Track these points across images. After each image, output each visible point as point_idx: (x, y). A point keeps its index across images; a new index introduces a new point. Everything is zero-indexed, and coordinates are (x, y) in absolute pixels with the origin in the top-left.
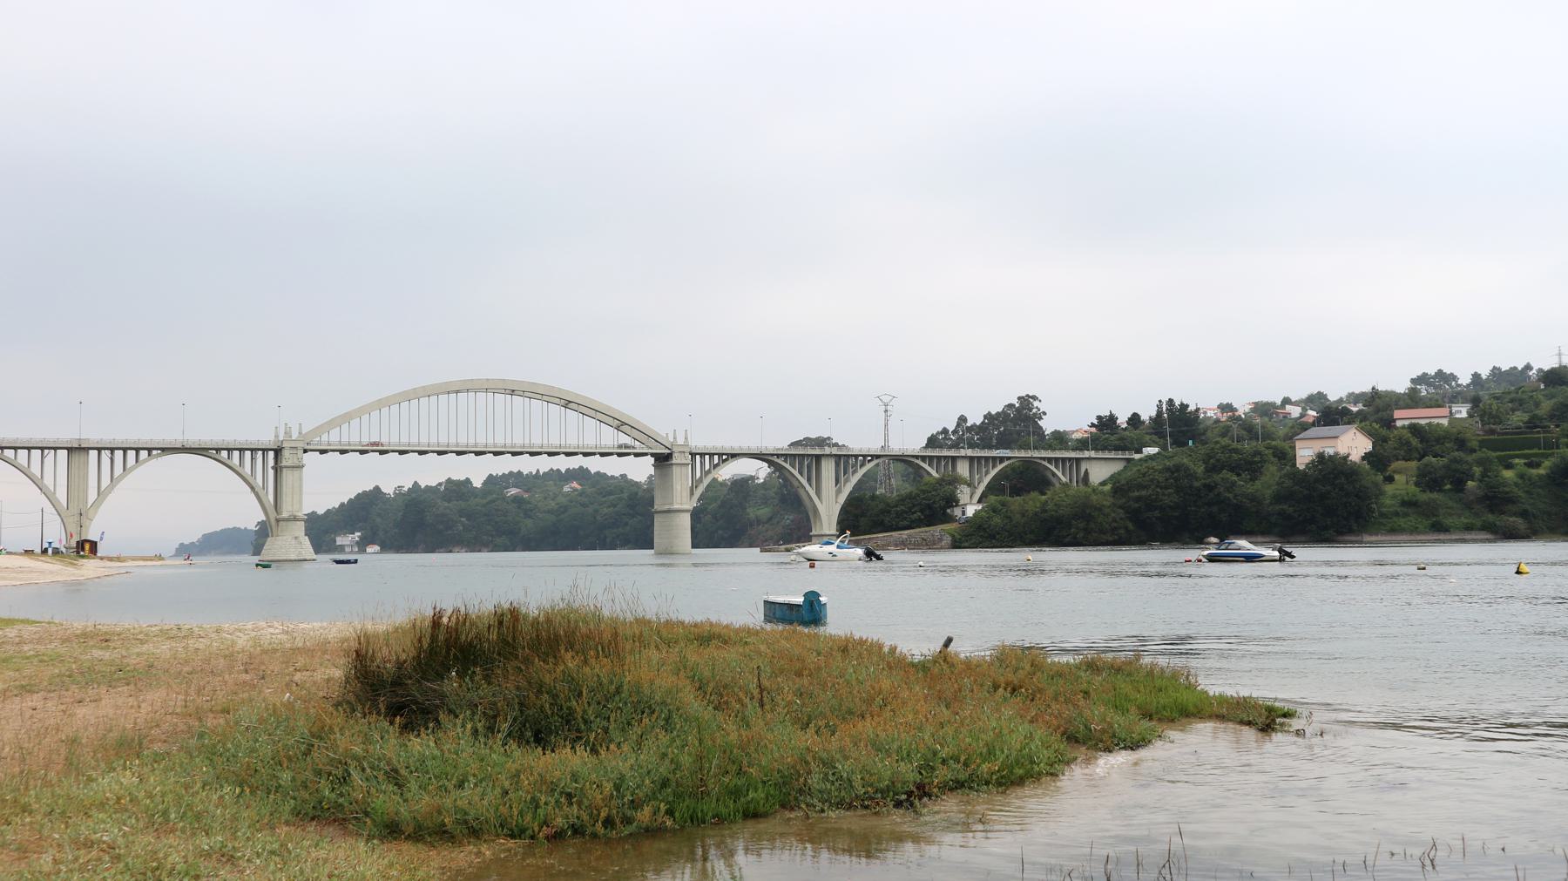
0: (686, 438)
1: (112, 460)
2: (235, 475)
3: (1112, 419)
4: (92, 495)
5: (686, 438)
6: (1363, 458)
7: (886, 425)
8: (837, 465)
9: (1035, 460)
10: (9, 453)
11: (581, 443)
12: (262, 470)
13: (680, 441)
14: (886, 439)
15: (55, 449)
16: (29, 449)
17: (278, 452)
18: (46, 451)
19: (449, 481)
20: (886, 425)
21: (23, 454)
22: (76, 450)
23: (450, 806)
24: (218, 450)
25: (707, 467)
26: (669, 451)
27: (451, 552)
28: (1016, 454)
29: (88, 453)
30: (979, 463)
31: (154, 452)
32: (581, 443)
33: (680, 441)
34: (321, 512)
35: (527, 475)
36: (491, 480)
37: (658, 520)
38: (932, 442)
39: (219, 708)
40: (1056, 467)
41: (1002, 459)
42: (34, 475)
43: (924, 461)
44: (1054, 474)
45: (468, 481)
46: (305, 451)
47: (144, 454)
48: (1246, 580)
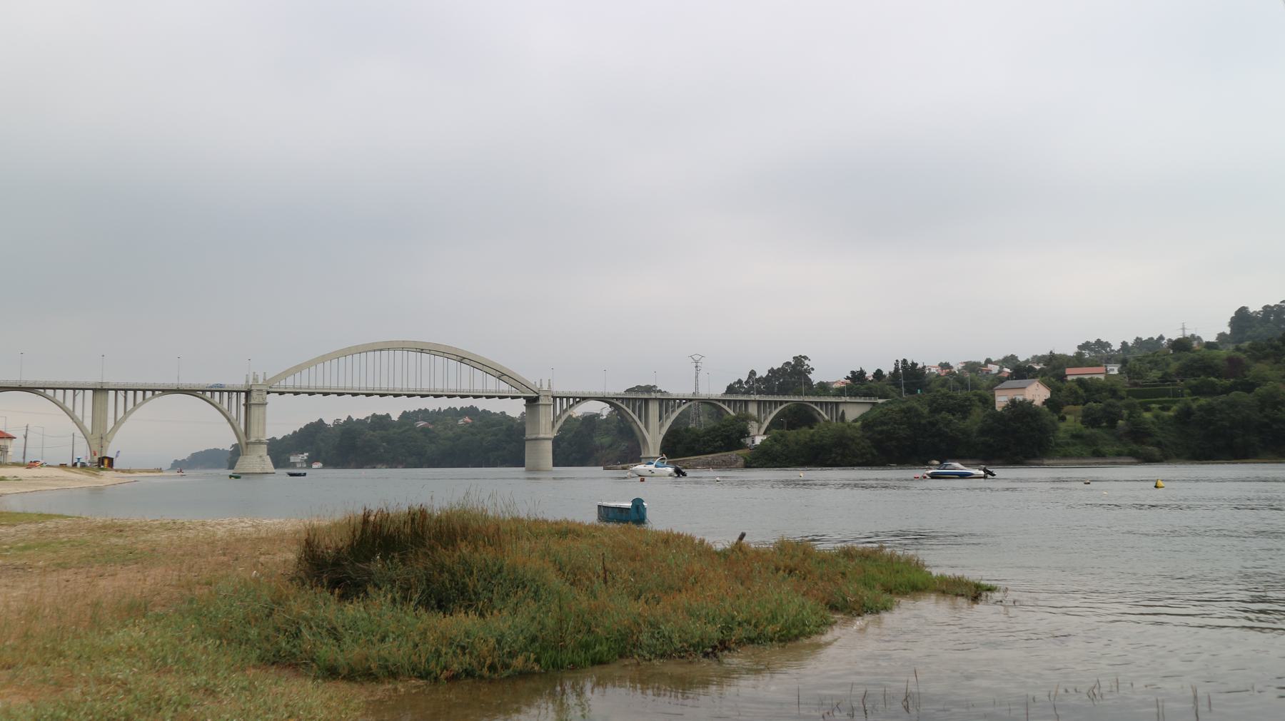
0: (549, 386)
1: (125, 398)
4: (110, 424)
5: (549, 386)
7: (697, 377)
10: (50, 392)
12: (236, 406)
17: (248, 393)
18: (77, 391)
20: (697, 377)
24: (204, 391)
27: (374, 468)
30: (765, 406)
31: (157, 393)
36: (405, 415)
37: (528, 445)
40: (821, 409)
43: (724, 403)
46: (268, 393)
47: (149, 394)
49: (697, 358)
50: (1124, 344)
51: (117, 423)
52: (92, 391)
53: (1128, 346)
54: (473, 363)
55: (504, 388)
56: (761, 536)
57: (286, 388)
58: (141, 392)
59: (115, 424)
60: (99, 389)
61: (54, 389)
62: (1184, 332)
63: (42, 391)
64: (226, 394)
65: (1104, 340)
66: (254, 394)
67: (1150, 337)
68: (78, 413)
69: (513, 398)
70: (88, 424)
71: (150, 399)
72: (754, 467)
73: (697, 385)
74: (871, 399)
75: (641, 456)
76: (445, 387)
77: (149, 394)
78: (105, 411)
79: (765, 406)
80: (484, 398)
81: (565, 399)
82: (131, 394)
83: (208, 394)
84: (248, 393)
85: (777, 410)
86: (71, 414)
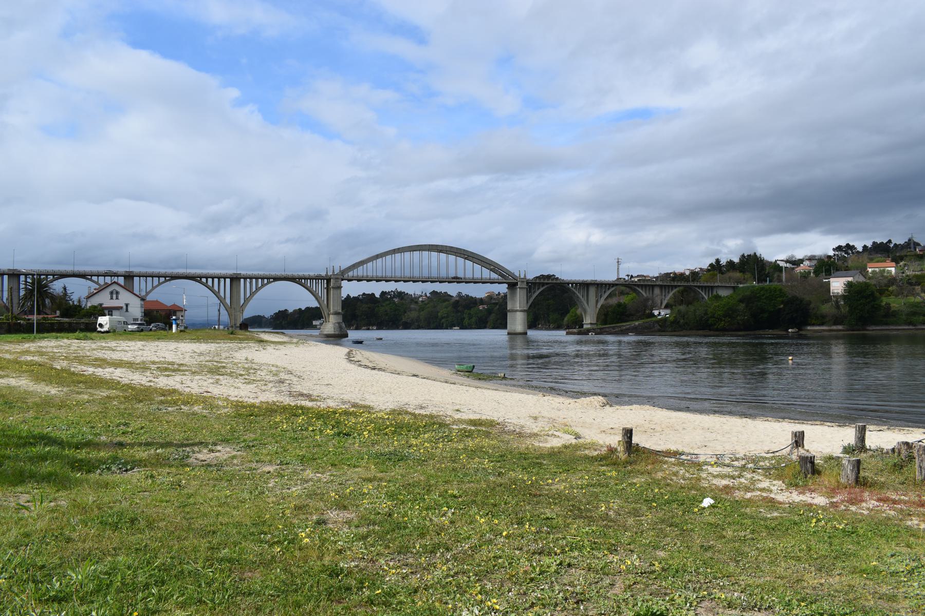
0: (525, 275)
2: (306, 290)
3: (712, 264)
4: (242, 301)
5: (525, 275)
7: (618, 269)
8: (597, 288)
10: (95, 278)
12: (320, 288)
13: (522, 276)
14: (327, 273)
15: (146, 277)
16: (310, 279)
17: (328, 281)
18: (113, 277)
19: (364, 294)
20: (618, 269)
22: (235, 279)
23: (895, 359)
24: (201, 278)
25: (254, 289)
27: (368, 329)
30: (665, 288)
31: (167, 278)
32: (403, 275)
34: (291, 310)
36: (383, 294)
37: (509, 314)
40: (702, 290)
43: (699, 288)
44: (578, 297)
45: (373, 294)
46: (342, 280)
47: (266, 281)
51: (247, 300)
52: (123, 278)
54: (474, 260)
55: (494, 276)
56: (125, 381)
59: (245, 301)
63: (90, 277)
64: (248, 280)
65: (851, 244)
68: (222, 294)
69: (499, 283)
71: (267, 284)
73: (618, 274)
76: (393, 275)
77: (266, 281)
78: (239, 292)
79: (665, 288)
81: (260, 280)
82: (254, 280)
83: (303, 281)
84: (328, 281)
85: (540, 290)
86: (217, 294)
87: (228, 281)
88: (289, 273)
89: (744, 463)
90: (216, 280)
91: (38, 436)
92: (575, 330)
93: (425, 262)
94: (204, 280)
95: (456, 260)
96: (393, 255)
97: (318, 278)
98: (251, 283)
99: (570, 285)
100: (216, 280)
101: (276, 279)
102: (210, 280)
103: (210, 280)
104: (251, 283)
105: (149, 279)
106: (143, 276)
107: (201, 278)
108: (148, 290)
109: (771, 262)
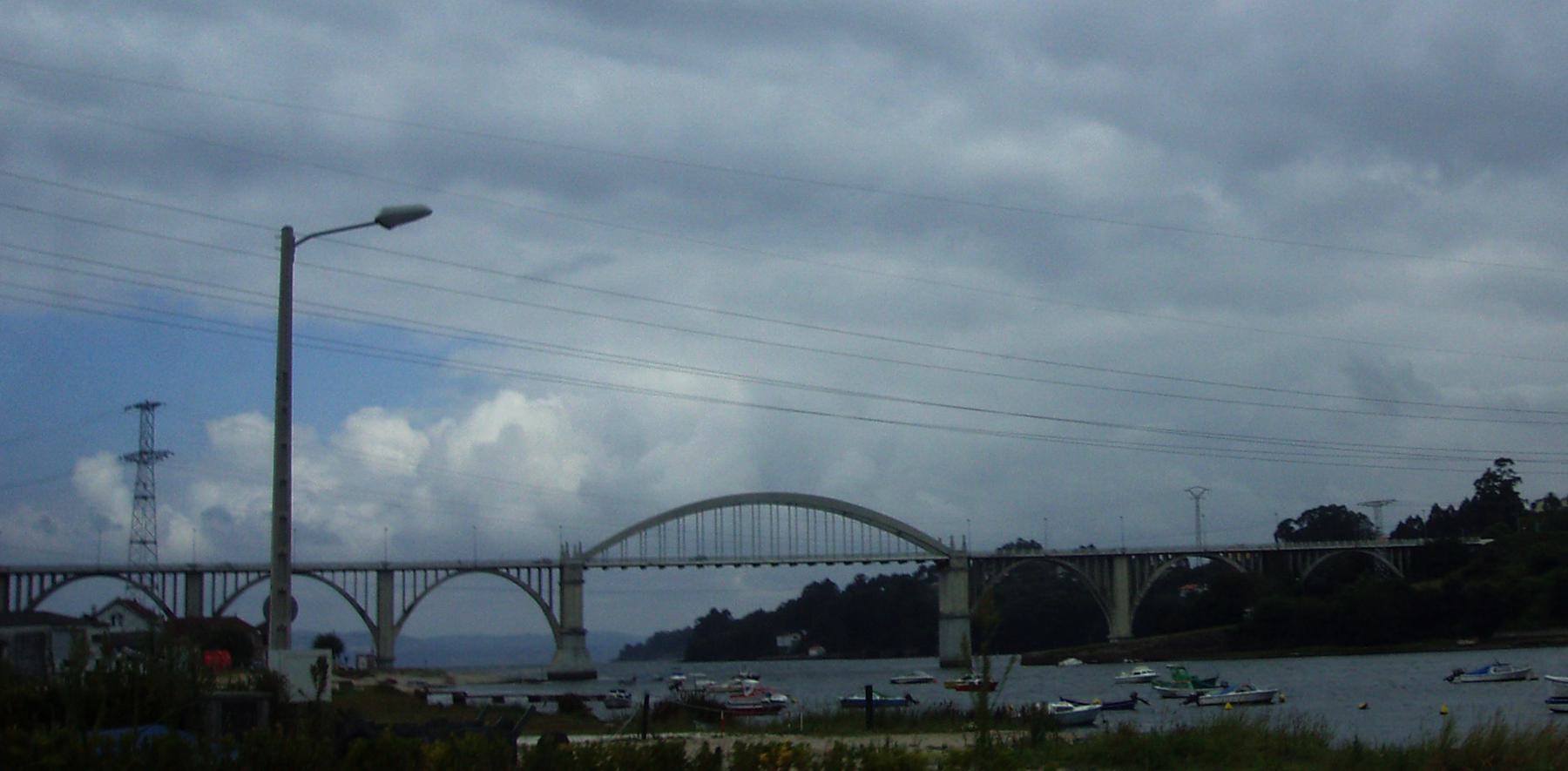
0: (964, 544)
1: (550, 575)
4: (398, 614)
5: (964, 544)
6: (1276, 536)
9: (1366, 552)
10: (328, 576)
11: (662, 556)
13: (958, 547)
21: (339, 575)
22: (385, 572)
24: (129, 573)
26: (946, 558)
28: (1337, 545)
29: (393, 574)
31: (451, 572)
33: (958, 547)
34: (738, 613)
35: (850, 587)
38: (1284, 530)
39: (139, 539)
41: (1321, 552)
42: (523, 583)
48: (1170, 702)
49: (1197, 491)
50: (1517, 493)
53: (837, 591)
57: (889, 555)
58: (526, 570)
60: (1119, 555)
61: (333, 571)
62: (1198, 539)
66: (567, 570)
67: (308, 671)
70: (372, 614)
72: (1296, 656)
74: (1317, 545)
75: (1109, 637)
80: (878, 564)
87: (181, 578)
88: (485, 557)
89: (1456, 678)
90: (535, 572)
91: (575, 746)
92: (1296, 654)
93: (765, 523)
94: (513, 572)
95: (789, 509)
96: (700, 514)
97: (544, 564)
98: (19, 581)
99: (1161, 557)
100: (535, 572)
101: (462, 569)
102: (524, 572)
103: (524, 572)
104: (19, 581)
105: (420, 574)
106: (361, 570)
107: (129, 573)
108: (429, 584)
109: (688, 630)
